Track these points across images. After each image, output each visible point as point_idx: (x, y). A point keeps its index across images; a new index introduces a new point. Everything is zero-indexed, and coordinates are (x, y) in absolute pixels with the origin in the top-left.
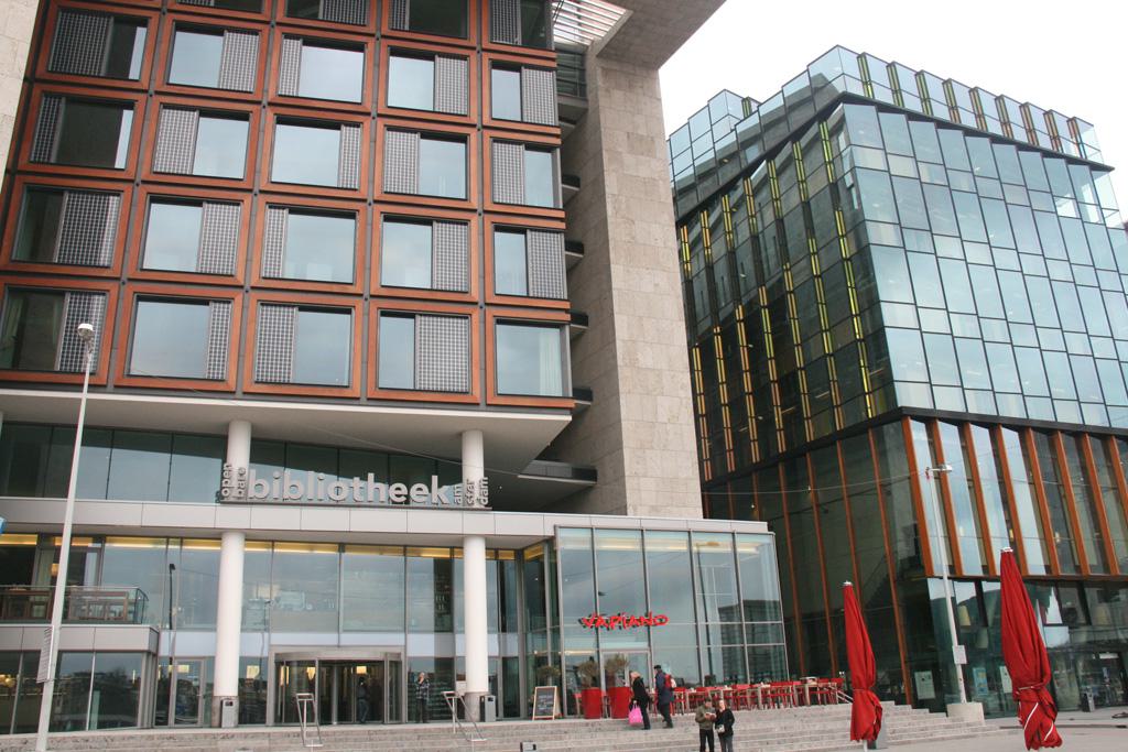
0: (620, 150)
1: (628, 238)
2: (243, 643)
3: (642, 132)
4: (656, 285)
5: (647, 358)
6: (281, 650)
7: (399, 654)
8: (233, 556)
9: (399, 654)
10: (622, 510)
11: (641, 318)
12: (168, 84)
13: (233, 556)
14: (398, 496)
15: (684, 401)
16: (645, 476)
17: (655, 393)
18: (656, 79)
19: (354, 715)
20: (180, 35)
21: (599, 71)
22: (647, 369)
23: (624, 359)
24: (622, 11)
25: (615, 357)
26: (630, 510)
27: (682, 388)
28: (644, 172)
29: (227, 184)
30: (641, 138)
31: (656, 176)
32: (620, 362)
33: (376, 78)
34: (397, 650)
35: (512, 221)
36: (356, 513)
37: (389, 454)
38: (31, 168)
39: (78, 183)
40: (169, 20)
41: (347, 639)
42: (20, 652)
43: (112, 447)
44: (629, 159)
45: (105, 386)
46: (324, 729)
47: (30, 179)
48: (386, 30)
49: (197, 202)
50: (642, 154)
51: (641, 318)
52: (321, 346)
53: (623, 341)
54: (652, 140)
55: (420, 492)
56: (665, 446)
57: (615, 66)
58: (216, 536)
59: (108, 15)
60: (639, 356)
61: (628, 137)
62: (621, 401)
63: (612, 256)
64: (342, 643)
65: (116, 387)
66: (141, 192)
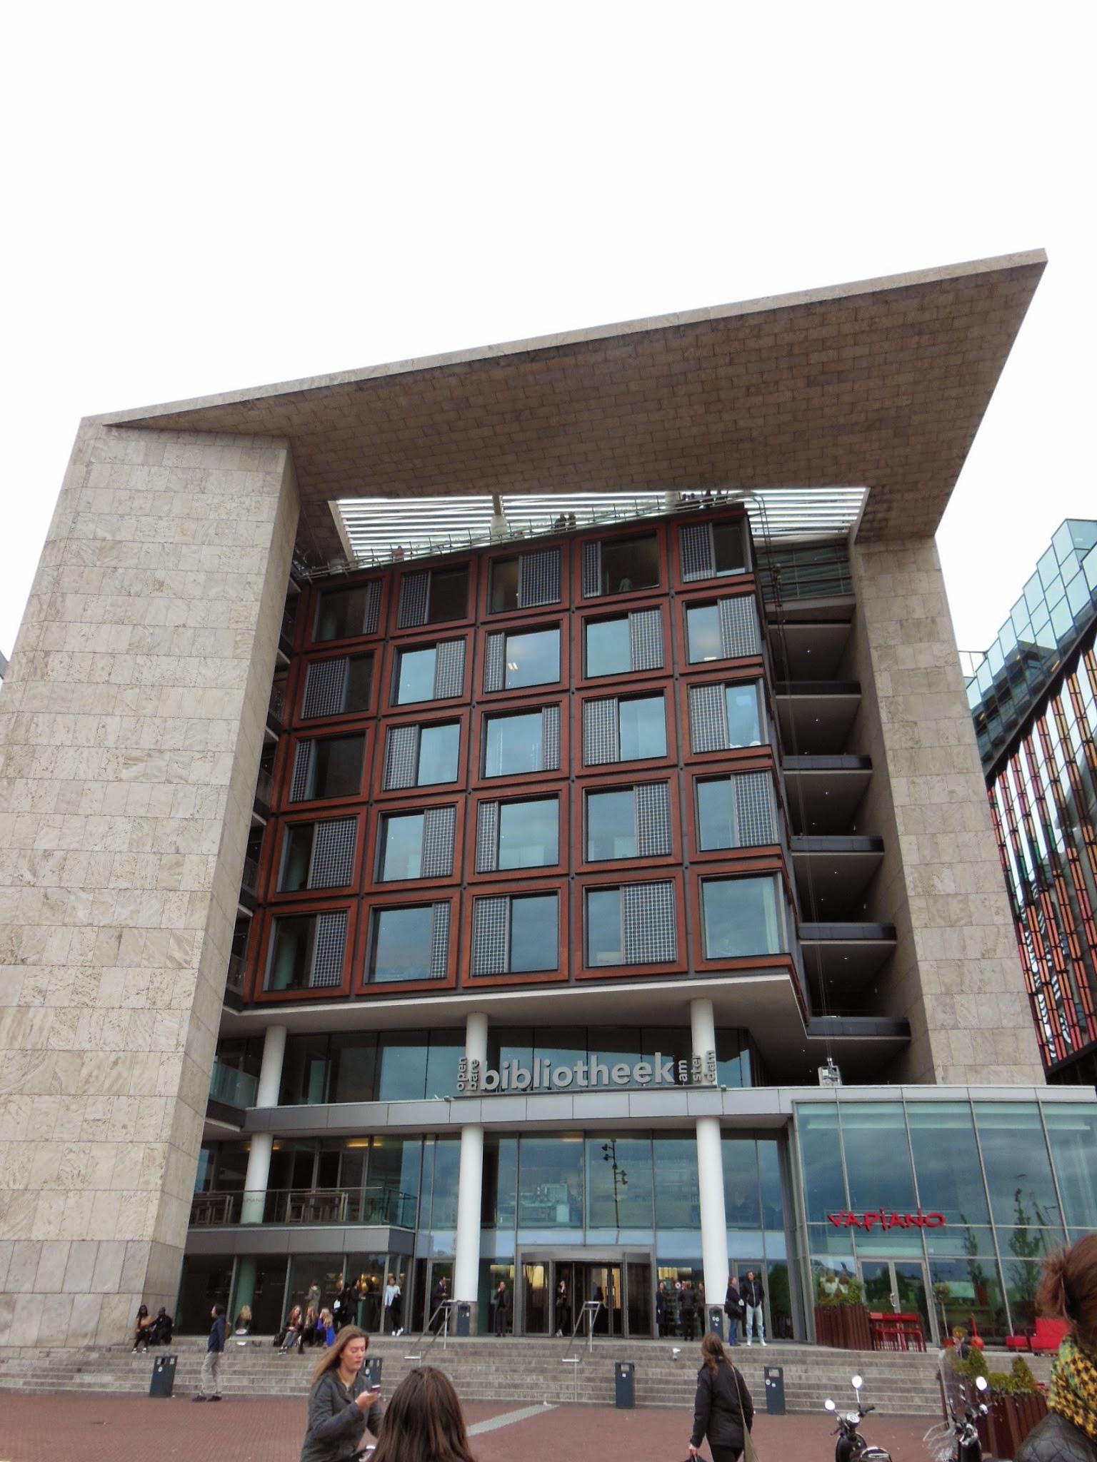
0: (891, 643)
1: (910, 744)
2: (699, 1244)
3: (919, 614)
4: (952, 792)
5: (946, 883)
6: (527, 1250)
7: (648, 1255)
8: (709, 1142)
9: (648, 1255)
10: (927, 1077)
11: (934, 835)
12: (587, 678)
13: (709, 1142)
14: (642, 1076)
15: (1002, 929)
16: (955, 1027)
17: (962, 922)
18: (934, 546)
19: (656, 1327)
20: (691, 612)
21: (860, 559)
22: (948, 895)
23: (915, 887)
24: (863, 490)
25: (904, 887)
26: (939, 1073)
27: (997, 913)
28: (925, 661)
29: (645, 765)
30: (918, 624)
31: (941, 663)
32: (910, 892)
33: (574, 652)
34: (646, 1250)
35: (719, 766)
36: (635, 1096)
37: (641, 1029)
38: (291, 808)
39: (325, 814)
40: (577, 618)
41: (595, 1237)
42: (342, 1254)
43: (428, 1045)
44: (904, 652)
45: (686, 973)
46: (414, 1339)
47: (288, 818)
48: (483, 617)
49: (628, 787)
50: (921, 640)
51: (934, 835)
52: (535, 929)
53: (913, 866)
54: (933, 621)
55: (642, 1072)
56: (980, 988)
57: (878, 547)
58: (454, 1133)
59: (342, 657)
60: (936, 882)
61: (902, 625)
62: (916, 938)
63: (891, 768)
64: (589, 1242)
65: (357, 995)
66: (685, 776)
